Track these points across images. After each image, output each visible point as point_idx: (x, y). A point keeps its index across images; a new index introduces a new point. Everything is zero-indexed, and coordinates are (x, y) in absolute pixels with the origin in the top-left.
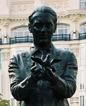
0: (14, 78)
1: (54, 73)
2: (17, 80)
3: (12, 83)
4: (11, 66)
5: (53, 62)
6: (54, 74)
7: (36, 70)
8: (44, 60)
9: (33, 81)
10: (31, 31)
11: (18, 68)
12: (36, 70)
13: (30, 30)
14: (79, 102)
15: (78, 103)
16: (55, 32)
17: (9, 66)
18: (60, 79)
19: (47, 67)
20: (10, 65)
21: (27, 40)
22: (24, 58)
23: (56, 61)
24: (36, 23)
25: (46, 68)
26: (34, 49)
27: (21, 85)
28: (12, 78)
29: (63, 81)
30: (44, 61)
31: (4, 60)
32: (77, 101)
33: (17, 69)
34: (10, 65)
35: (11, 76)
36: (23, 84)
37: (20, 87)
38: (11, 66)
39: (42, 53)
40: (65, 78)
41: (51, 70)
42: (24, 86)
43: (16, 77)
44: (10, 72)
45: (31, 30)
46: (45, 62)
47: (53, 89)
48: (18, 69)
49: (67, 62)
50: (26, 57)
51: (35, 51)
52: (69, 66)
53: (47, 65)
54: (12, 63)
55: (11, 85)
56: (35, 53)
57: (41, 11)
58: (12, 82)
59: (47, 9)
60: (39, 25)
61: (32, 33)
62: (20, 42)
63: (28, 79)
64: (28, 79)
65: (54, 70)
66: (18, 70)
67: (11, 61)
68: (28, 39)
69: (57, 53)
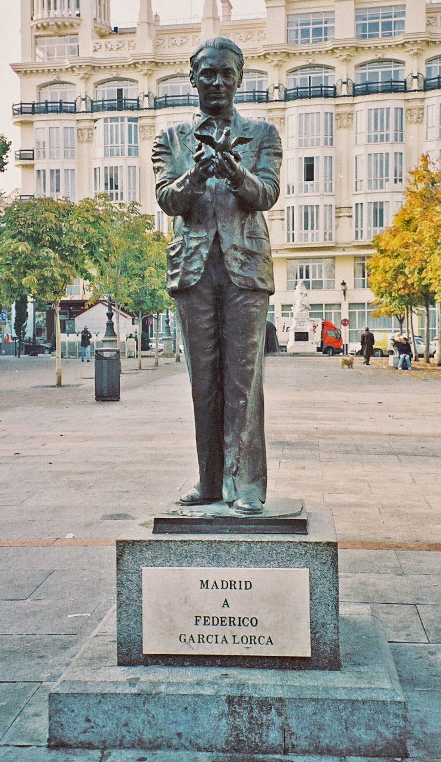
2: (169, 177)
3: (158, 182)
4: (158, 150)
5: (236, 143)
7: (203, 158)
10: (194, 84)
12: (203, 158)
14: (286, 217)
15: (283, 219)
17: (153, 151)
18: (249, 174)
19: (224, 153)
20: (155, 149)
21: (252, 98)
25: (222, 154)
28: (159, 173)
31: (144, 139)
32: (280, 217)
35: (157, 170)
42: (182, 188)
43: (165, 172)
47: (235, 194)
48: (169, 156)
56: (203, 126)
58: (159, 180)
60: (210, 72)
61: (196, 88)
62: (173, 105)
65: (237, 158)
68: (188, 99)
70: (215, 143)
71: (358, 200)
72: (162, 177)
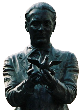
0: (9, 81)
1: (53, 76)
2: (13, 84)
3: (6, 87)
4: (6, 68)
5: (52, 64)
6: (53, 77)
7: (33, 73)
8: (42, 62)
9: (29, 85)
10: (28, 30)
11: (13, 71)
12: (33, 73)
13: (26, 29)
16: (54, 31)
17: (4, 69)
18: (59, 82)
20: (5, 68)
22: (20, 59)
23: (54, 63)
24: (33, 22)
25: (44, 71)
26: (31, 50)
27: (17, 90)
28: (7, 82)
29: (63, 85)
30: (42, 63)
33: (12, 72)
34: (5, 68)
35: (6, 80)
36: (18, 89)
37: (15, 92)
38: (6, 68)
39: (40, 54)
40: (65, 82)
41: (50, 72)
42: (21, 90)
44: (4, 75)
45: (28, 29)
46: (43, 64)
47: (51, 94)
49: (67, 64)
51: (32, 52)
52: (69, 69)
53: (45, 67)
54: (7, 66)
55: (6, 89)
56: (32, 55)
57: (39, 8)
59: (46, 6)
63: (25, 82)
64: (25, 82)
65: (53, 73)
66: (14, 73)
67: (6, 63)
69: (56, 54)
70: (40, 64)
72: (9, 84)
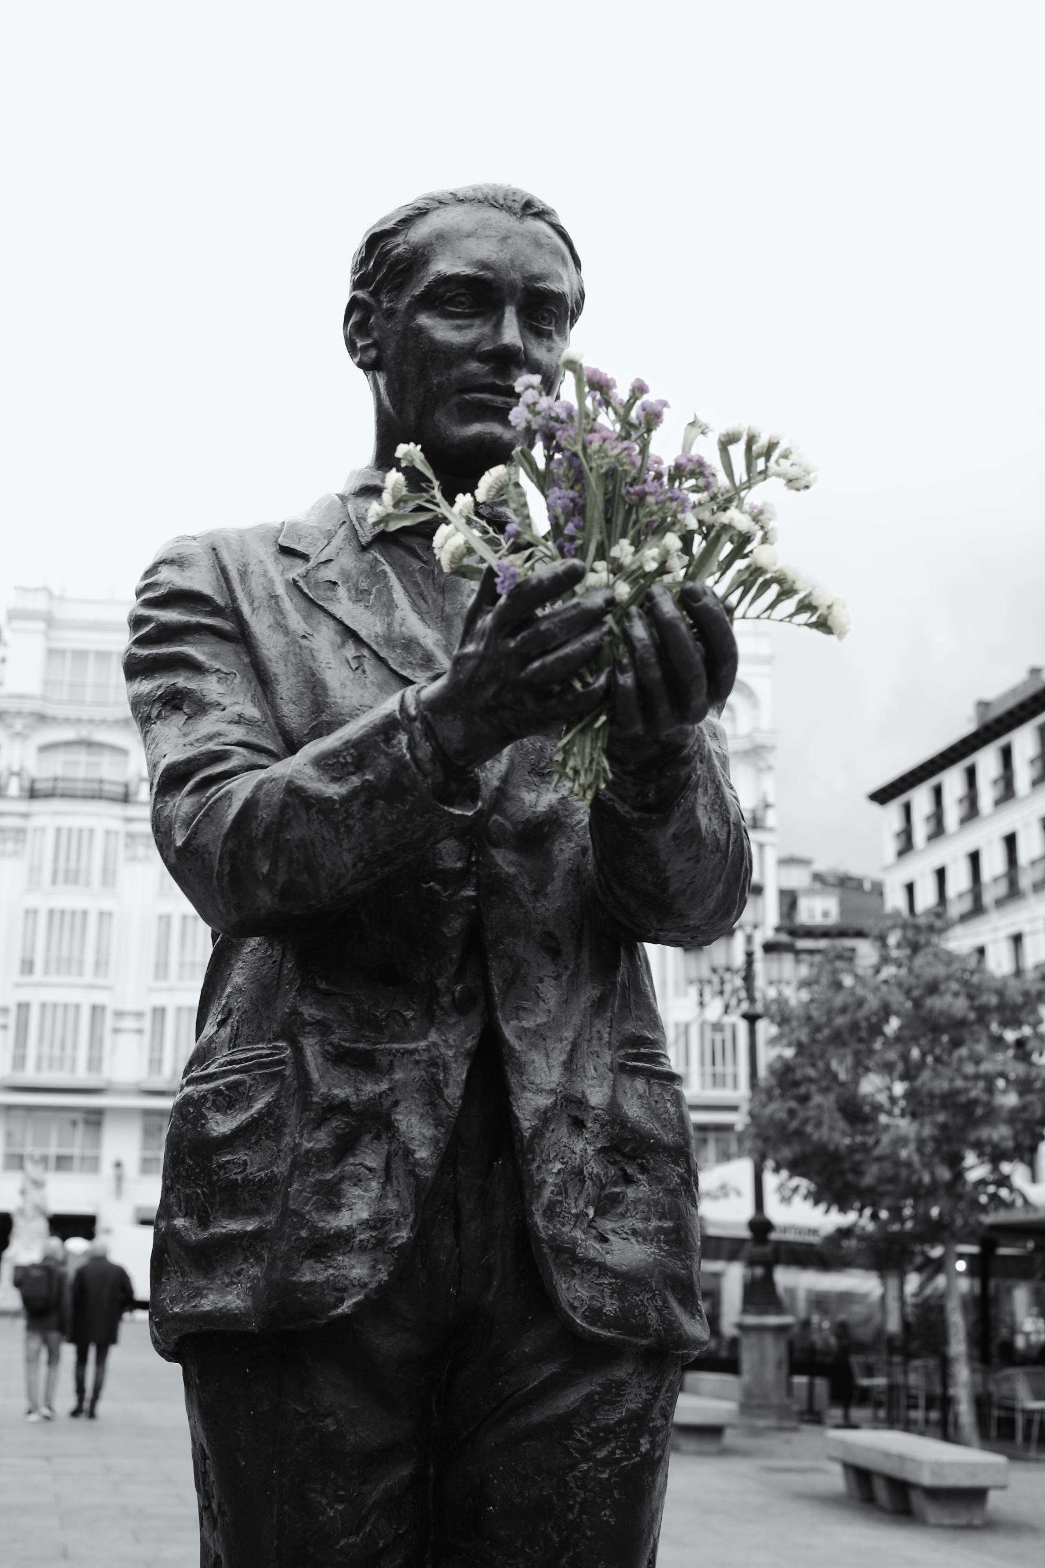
22: (286, 561)
50: (305, 557)
71: (23, 995)
